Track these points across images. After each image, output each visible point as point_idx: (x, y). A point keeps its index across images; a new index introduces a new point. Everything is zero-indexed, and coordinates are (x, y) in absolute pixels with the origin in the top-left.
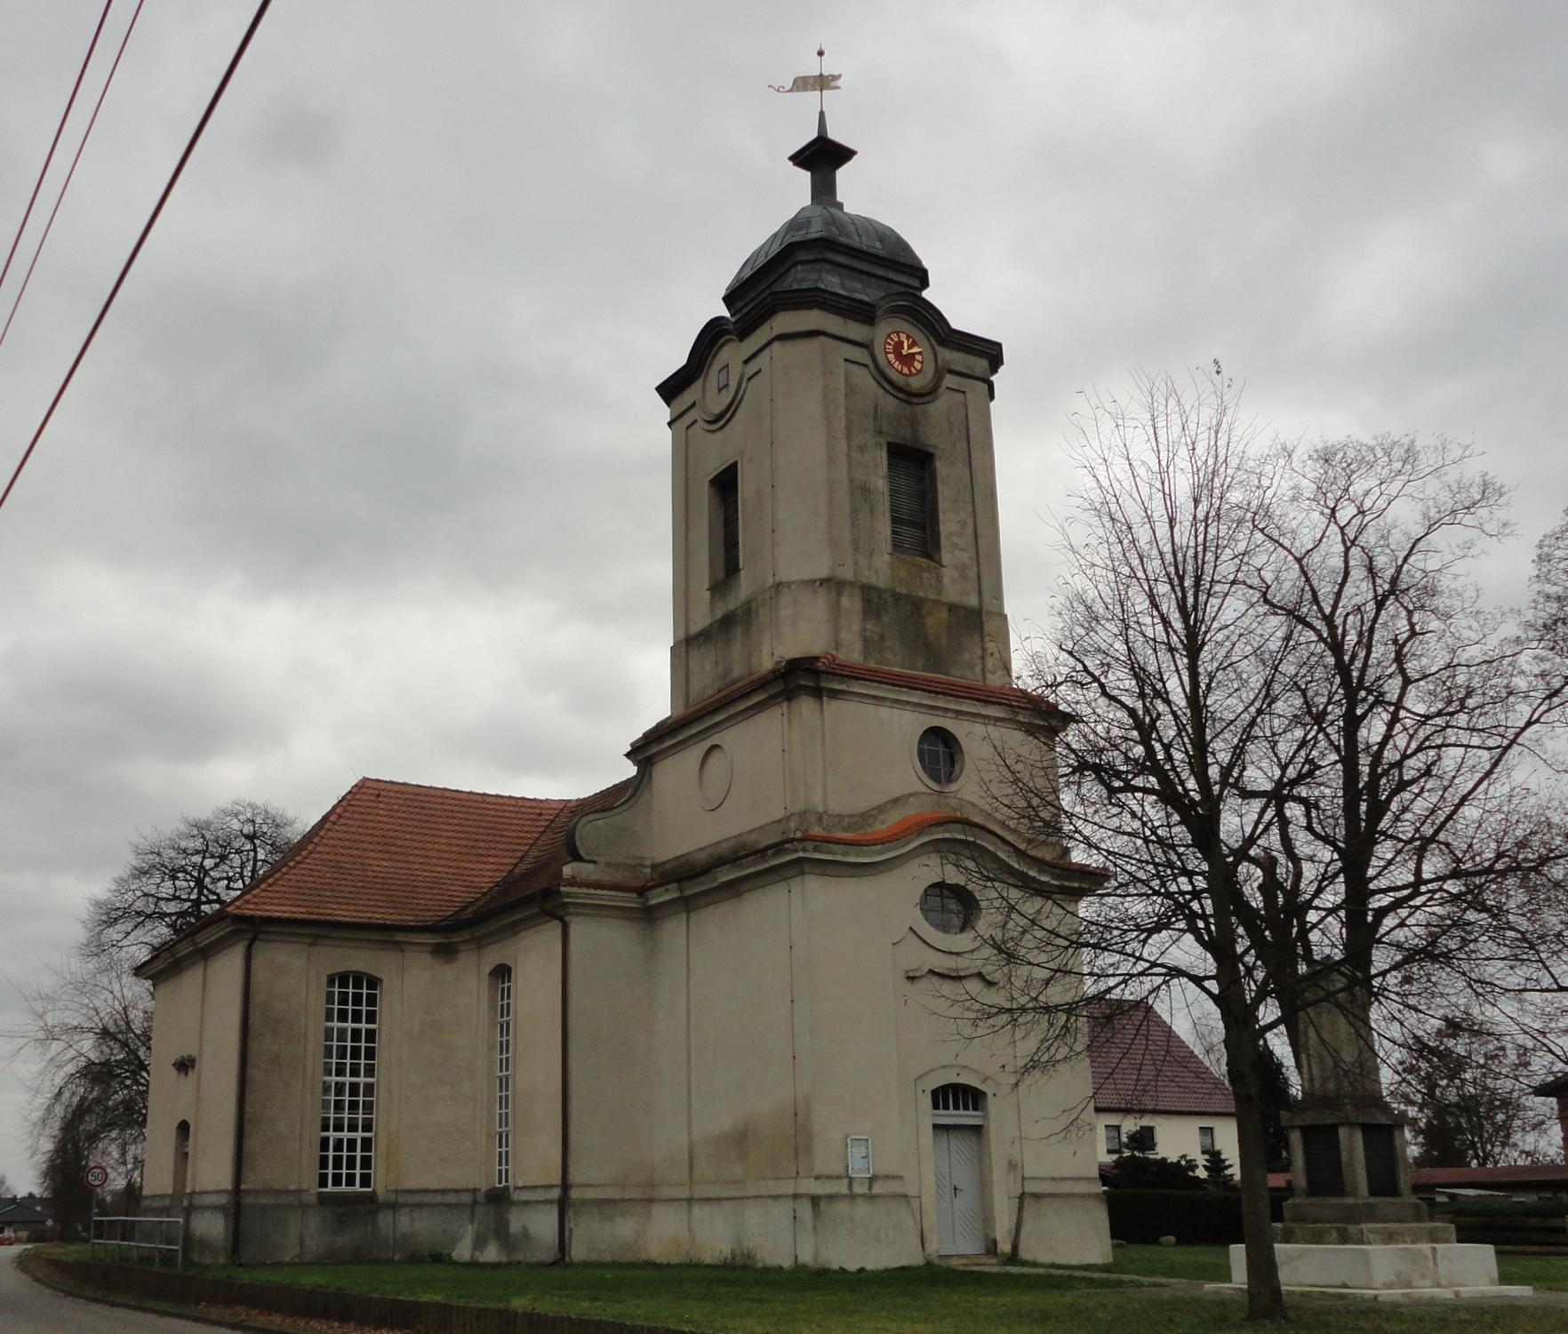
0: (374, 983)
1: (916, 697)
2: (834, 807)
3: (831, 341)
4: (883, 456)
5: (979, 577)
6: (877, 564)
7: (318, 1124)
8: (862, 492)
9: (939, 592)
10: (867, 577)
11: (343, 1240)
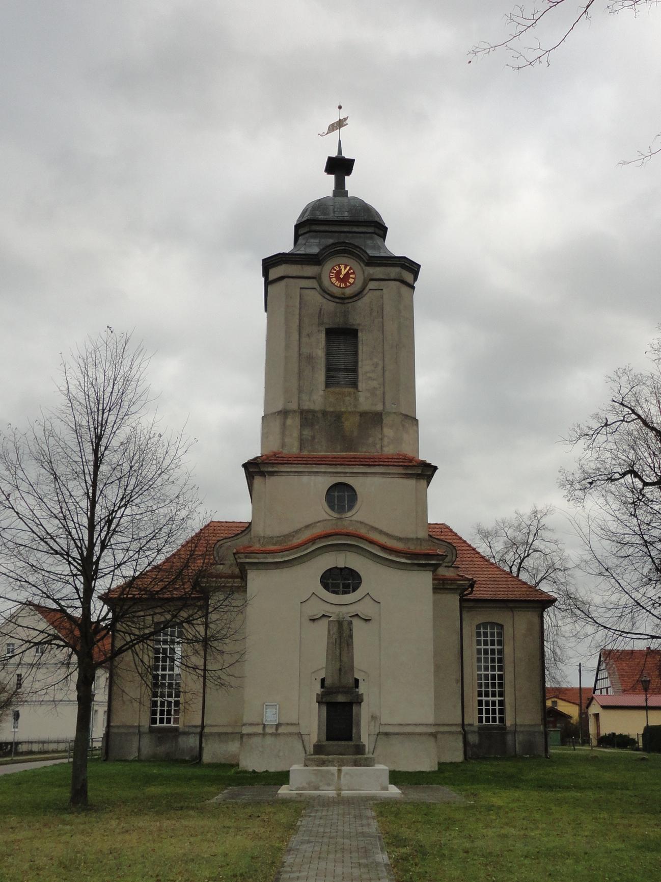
0: (501, 626)
1: (323, 469)
2: (269, 533)
3: (291, 280)
4: (323, 336)
5: (384, 393)
6: (315, 397)
7: (476, 694)
8: (307, 360)
9: (355, 406)
10: (306, 406)
11: (162, 750)
